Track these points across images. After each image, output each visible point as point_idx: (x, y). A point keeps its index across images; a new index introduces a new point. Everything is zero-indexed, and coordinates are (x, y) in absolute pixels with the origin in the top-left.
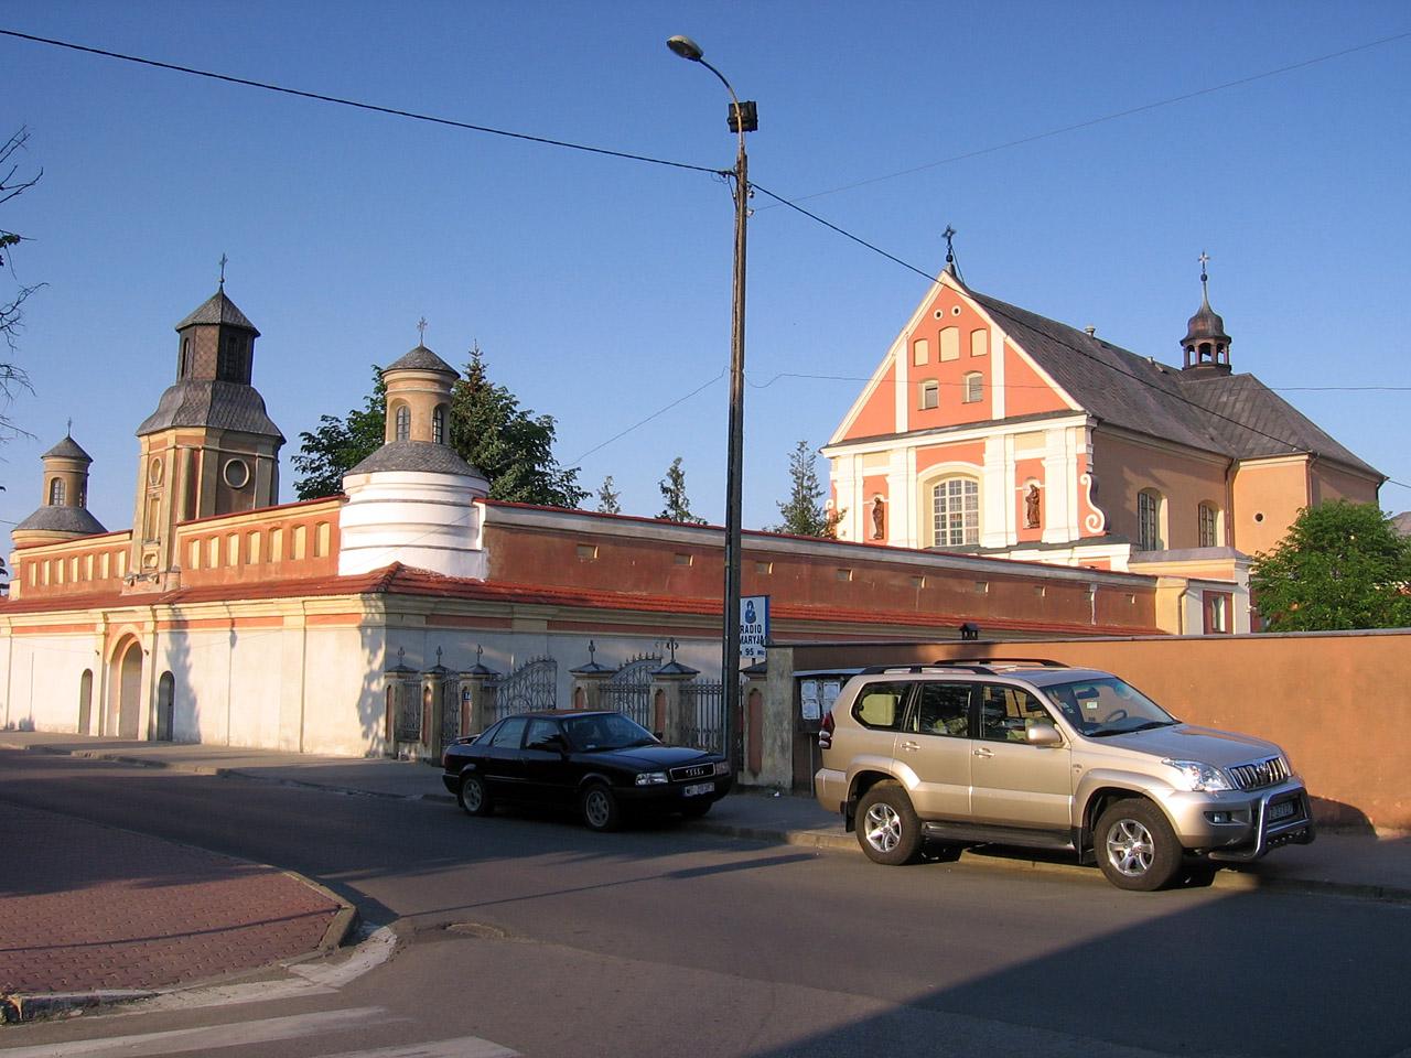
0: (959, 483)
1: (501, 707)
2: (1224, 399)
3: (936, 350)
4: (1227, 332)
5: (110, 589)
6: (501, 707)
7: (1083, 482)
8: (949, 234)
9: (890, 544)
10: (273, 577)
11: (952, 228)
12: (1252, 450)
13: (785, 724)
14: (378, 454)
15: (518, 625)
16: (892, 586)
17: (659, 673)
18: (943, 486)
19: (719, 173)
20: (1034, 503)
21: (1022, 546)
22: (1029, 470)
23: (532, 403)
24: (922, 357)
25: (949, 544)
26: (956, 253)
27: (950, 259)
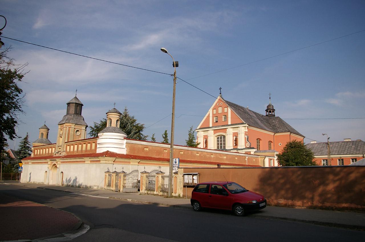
0: (222, 137)
1: (127, 180)
2: (273, 121)
3: (217, 111)
4: (274, 108)
5: (51, 155)
6: (127, 180)
7: (246, 137)
8: (220, 89)
9: (208, 148)
10: (83, 153)
12: (279, 131)
13: (181, 184)
14: (105, 129)
15: (101, 162)
17: (157, 173)
18: (219, 137)
20: (236, 141)
21: (234, 149)
22: (236, 135)
23: (139, 122)
24: (215, 113)
25: (220, 148)
26: (221, 92)
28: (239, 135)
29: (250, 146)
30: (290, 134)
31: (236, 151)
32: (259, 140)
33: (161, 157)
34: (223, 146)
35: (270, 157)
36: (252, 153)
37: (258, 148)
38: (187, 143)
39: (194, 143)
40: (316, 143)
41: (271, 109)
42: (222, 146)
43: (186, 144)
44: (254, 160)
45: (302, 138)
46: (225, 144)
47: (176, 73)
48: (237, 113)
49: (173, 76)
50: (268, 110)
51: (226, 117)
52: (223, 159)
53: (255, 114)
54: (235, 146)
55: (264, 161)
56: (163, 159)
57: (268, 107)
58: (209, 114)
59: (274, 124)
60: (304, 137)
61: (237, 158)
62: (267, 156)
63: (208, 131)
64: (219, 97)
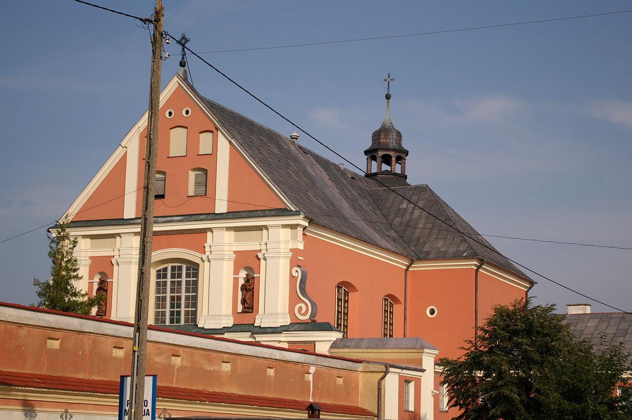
0: (180, 268)
2: (404, 206)
4: (405, 145)
7: (294, 274)
11: (187, 36)
12: (428, 253)
16: (157, 363)
18: (165, 269)
19: (141, 20)
21: (237, 328)
27: (182, 64)
28: (262, 261)
29: (313, 315)
30: (479, 267)
31: (245, 337)
32: (345, 288)
33: (171, 386)
34: (187, 313)
35: (406, 369)
36: (323, 348)
37: (341, 325)
38: (40, 294)
39: (75, 295)
40: (592, 315)
41: (391, 146)
42: (179, 313)
43: (36, 301)
44: (340, 381)
45: (522, 286)
46: (193, 301)
47: (165, 12)
48: (257, 164)
49: (152, 26)
50: (376, 150)
51: (206, 176)
52: (215, 376)
53: (326, 169)
54: (243, 312)
55: (379, 390)
56: (120, 386)
57: (377, 135)
58: (124, 158)
59: (405, 219)
60: (532, 283)
61: (229, 365)
62: (393, 366)
63: (113, 236)
64: (176, 79)
